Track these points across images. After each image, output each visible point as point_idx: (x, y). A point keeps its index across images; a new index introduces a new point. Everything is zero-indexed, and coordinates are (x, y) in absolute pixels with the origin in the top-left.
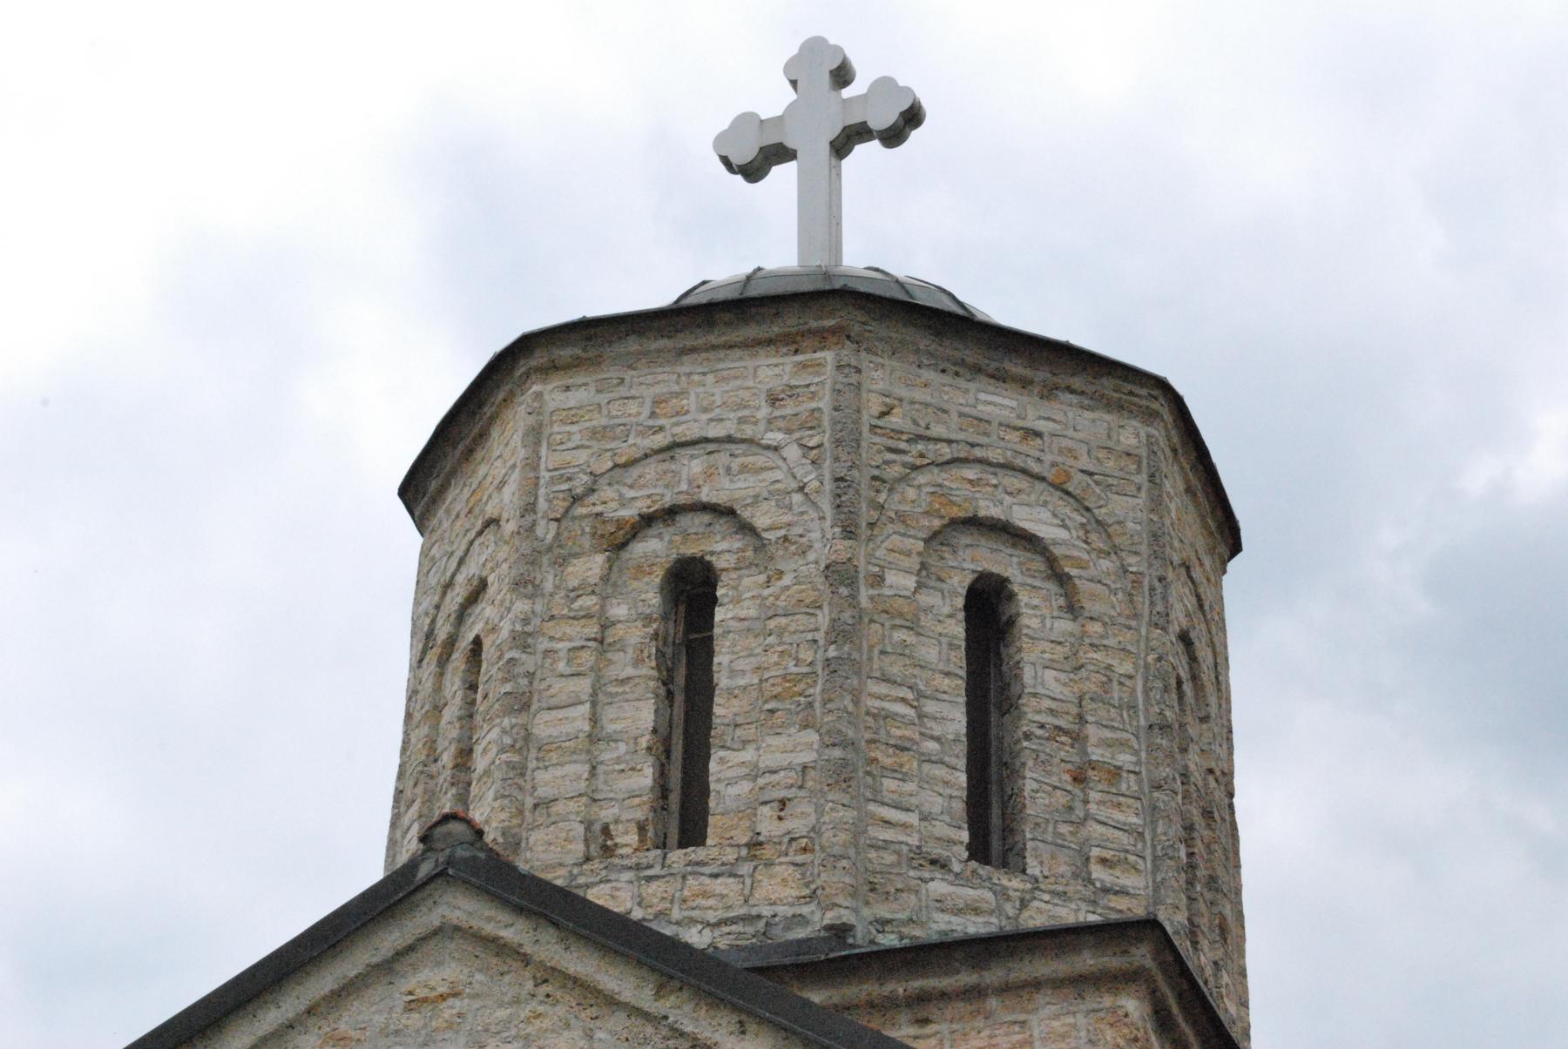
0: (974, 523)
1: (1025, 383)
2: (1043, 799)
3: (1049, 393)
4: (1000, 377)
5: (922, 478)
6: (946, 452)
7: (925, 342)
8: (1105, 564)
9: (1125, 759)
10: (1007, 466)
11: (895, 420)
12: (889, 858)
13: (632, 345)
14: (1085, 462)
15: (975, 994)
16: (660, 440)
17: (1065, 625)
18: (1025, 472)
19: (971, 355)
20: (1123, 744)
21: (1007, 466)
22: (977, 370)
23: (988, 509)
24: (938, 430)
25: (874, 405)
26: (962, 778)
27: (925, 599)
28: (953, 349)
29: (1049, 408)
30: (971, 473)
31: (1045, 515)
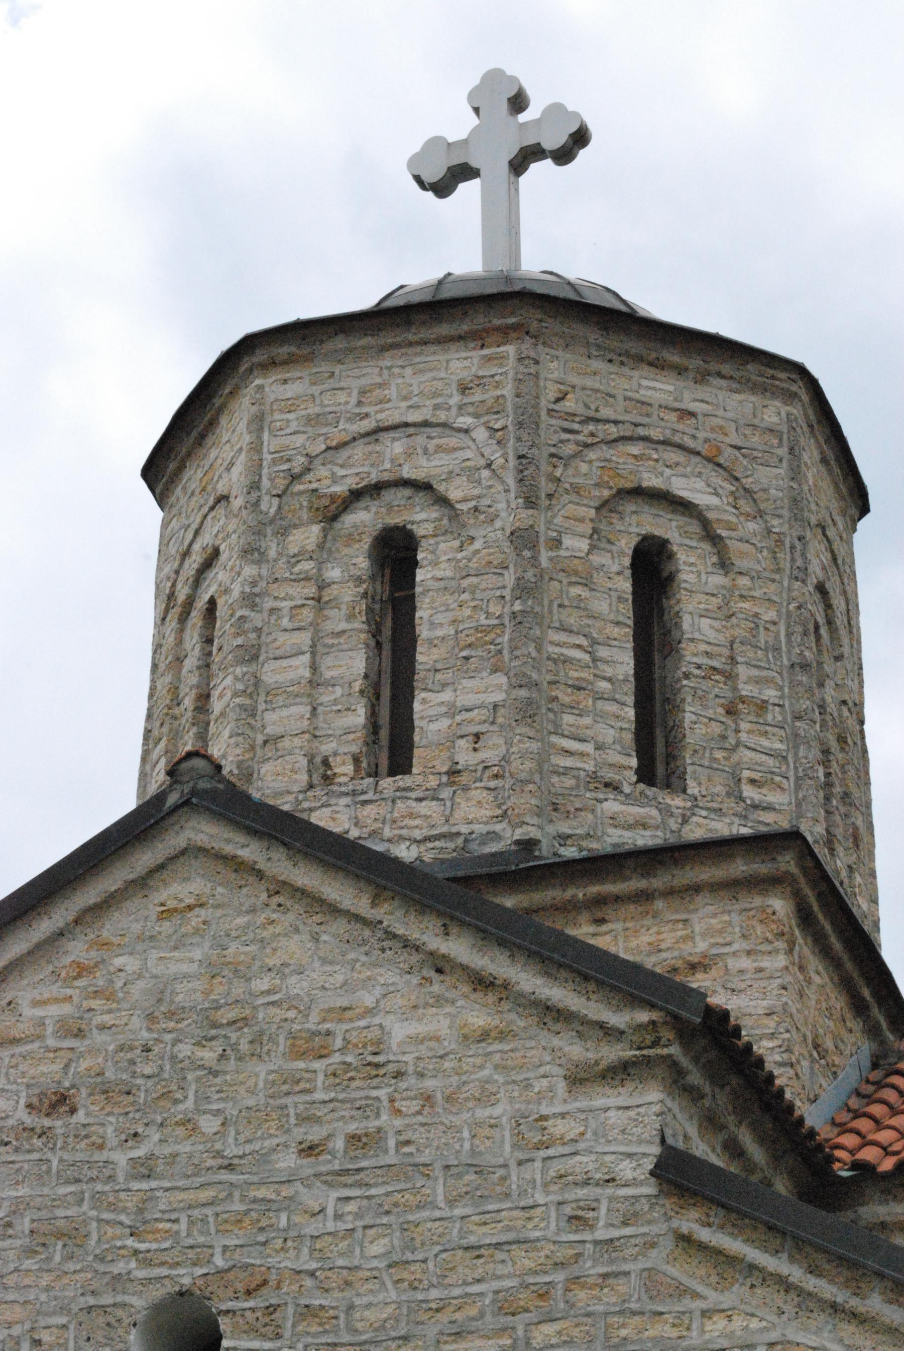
0: (639, 493)
1: (680, 371)
2: (700, 730)
3: (702, 378)
4: (658, 365)
5: (592, 455)
6: (613, 431)
7: (594, 335)
8: (752, 526)
9: (770, 694)
10: (664, 443)
11: (569, 404)
12: (569, 782)
13: (340, 343)
14: (734, 439)
15: (644, 897)
16: (367, 425)
17: (717, 580)
18: (681, 447)
19: (634, 346)
20: (768, 681)
21: (664, 443)
22: (639, 359)
23: (650, 481)
24: (606, 412)
25: (551, 391)
26: (631, 713)
27: (597, 559)
28: (615, 342)
29: (703, 392)
30: (635, 449)
31: (700, 484)
